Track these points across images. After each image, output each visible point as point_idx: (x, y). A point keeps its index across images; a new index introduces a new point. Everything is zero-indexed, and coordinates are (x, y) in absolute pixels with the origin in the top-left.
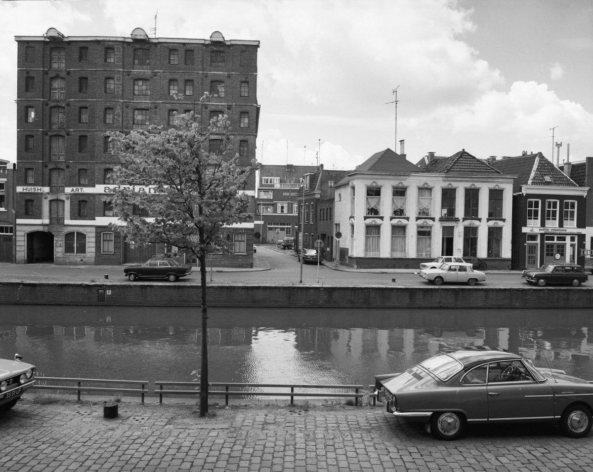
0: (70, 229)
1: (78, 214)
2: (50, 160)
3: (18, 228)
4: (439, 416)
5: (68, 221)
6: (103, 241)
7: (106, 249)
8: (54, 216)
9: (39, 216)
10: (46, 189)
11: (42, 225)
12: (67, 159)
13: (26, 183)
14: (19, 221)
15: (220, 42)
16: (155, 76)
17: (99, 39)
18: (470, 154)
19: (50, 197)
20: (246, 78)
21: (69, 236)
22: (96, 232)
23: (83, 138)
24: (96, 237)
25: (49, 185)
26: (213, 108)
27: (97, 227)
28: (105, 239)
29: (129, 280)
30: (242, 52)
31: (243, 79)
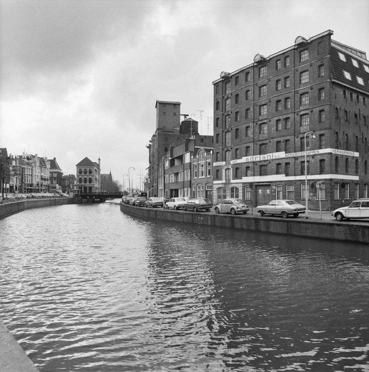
0: (232, 185)
1: (236, 177)
2: (225, 146)
3: (214, 186)
4: (316, 355)
5: (232, 181)
6: (303, 190)
7: (248, 198)
8: (227, 178)
9: (221, 180)
10: (224, 163)
11: (222, 184)
12: (232, 144)
13: (217, 161)
14: (215, 182)
15: (302, 43)
16: (269, 81)
17: (242, 69)
18: (149, 155)
19: (226, 168)
20: (322, 62)
21: (232, 189)
22: (243, 187)
23: (237, 130)
24: (243, 190)
25: (225, 161)
26: (302, 92)
27: (243, 183)
28: (278, 190)
29: (337, 220)
30: (319, 43)
31: (320, 64)
